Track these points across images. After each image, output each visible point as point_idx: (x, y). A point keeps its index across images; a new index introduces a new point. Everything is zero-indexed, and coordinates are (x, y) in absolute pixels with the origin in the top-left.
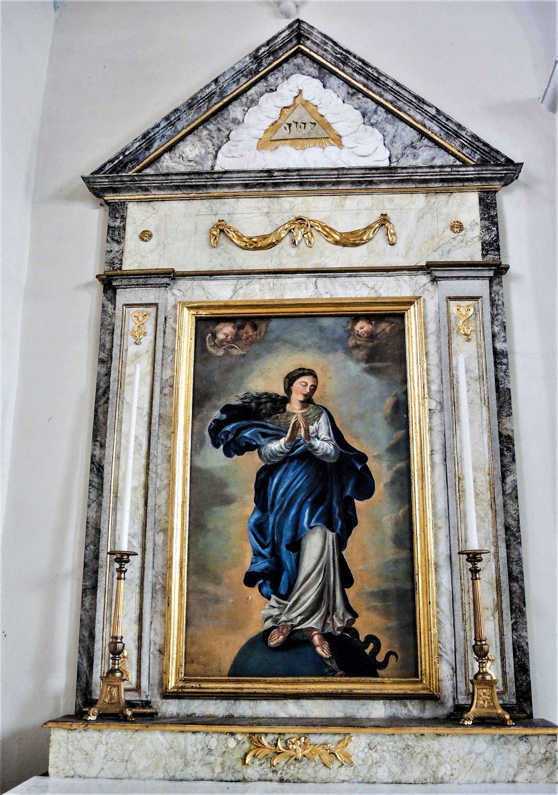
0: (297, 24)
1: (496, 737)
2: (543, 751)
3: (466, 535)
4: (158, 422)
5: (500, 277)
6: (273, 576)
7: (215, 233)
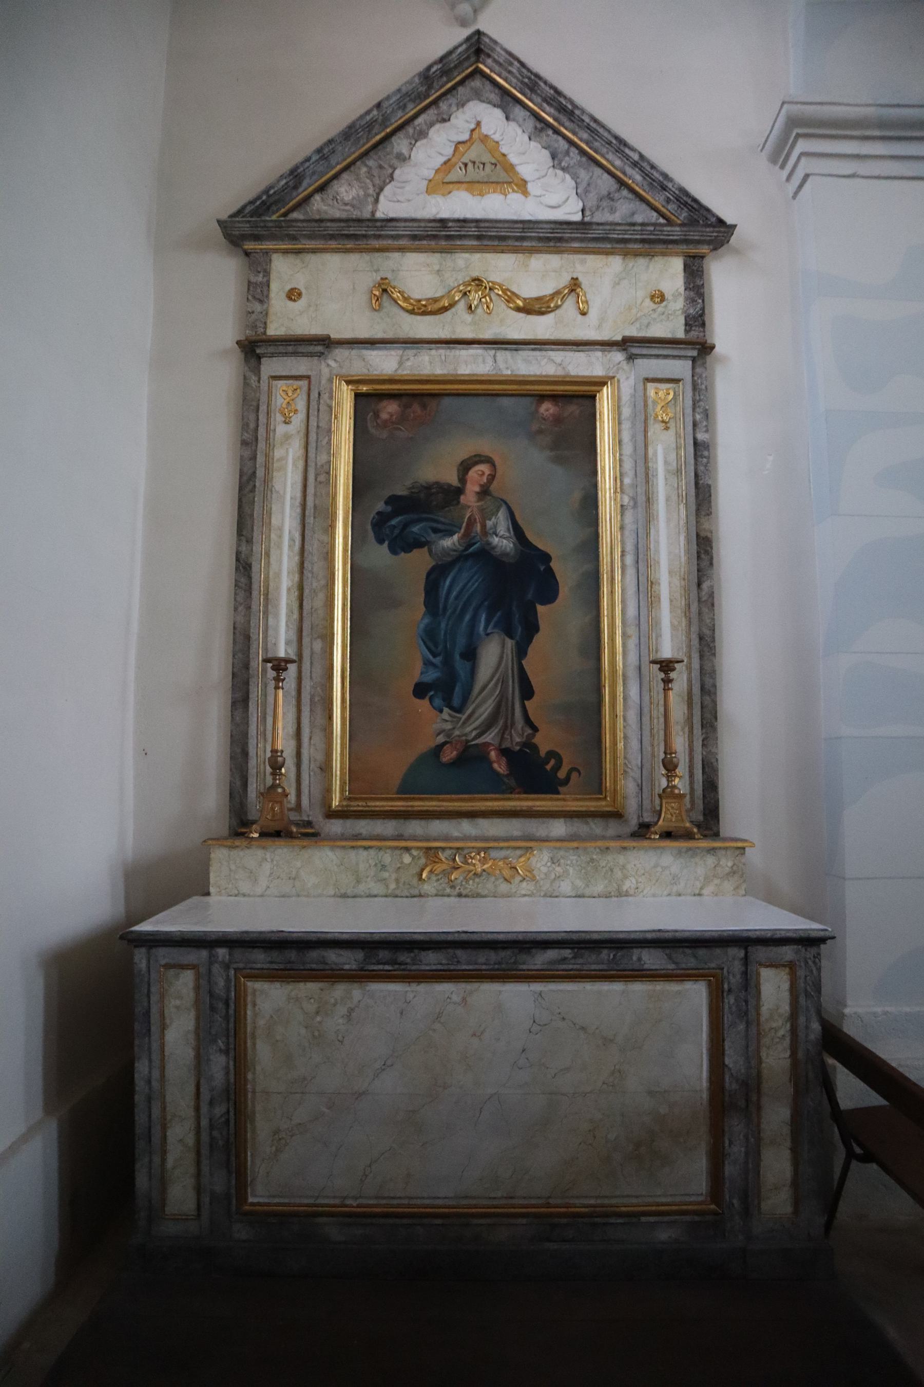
0: (477, 37)
1: (684, 850)
2: (730, 864)
3: (657, 644)
4: (314, 515)
5: (704, 358)
6: (445, 687)
7: (377, 293)
